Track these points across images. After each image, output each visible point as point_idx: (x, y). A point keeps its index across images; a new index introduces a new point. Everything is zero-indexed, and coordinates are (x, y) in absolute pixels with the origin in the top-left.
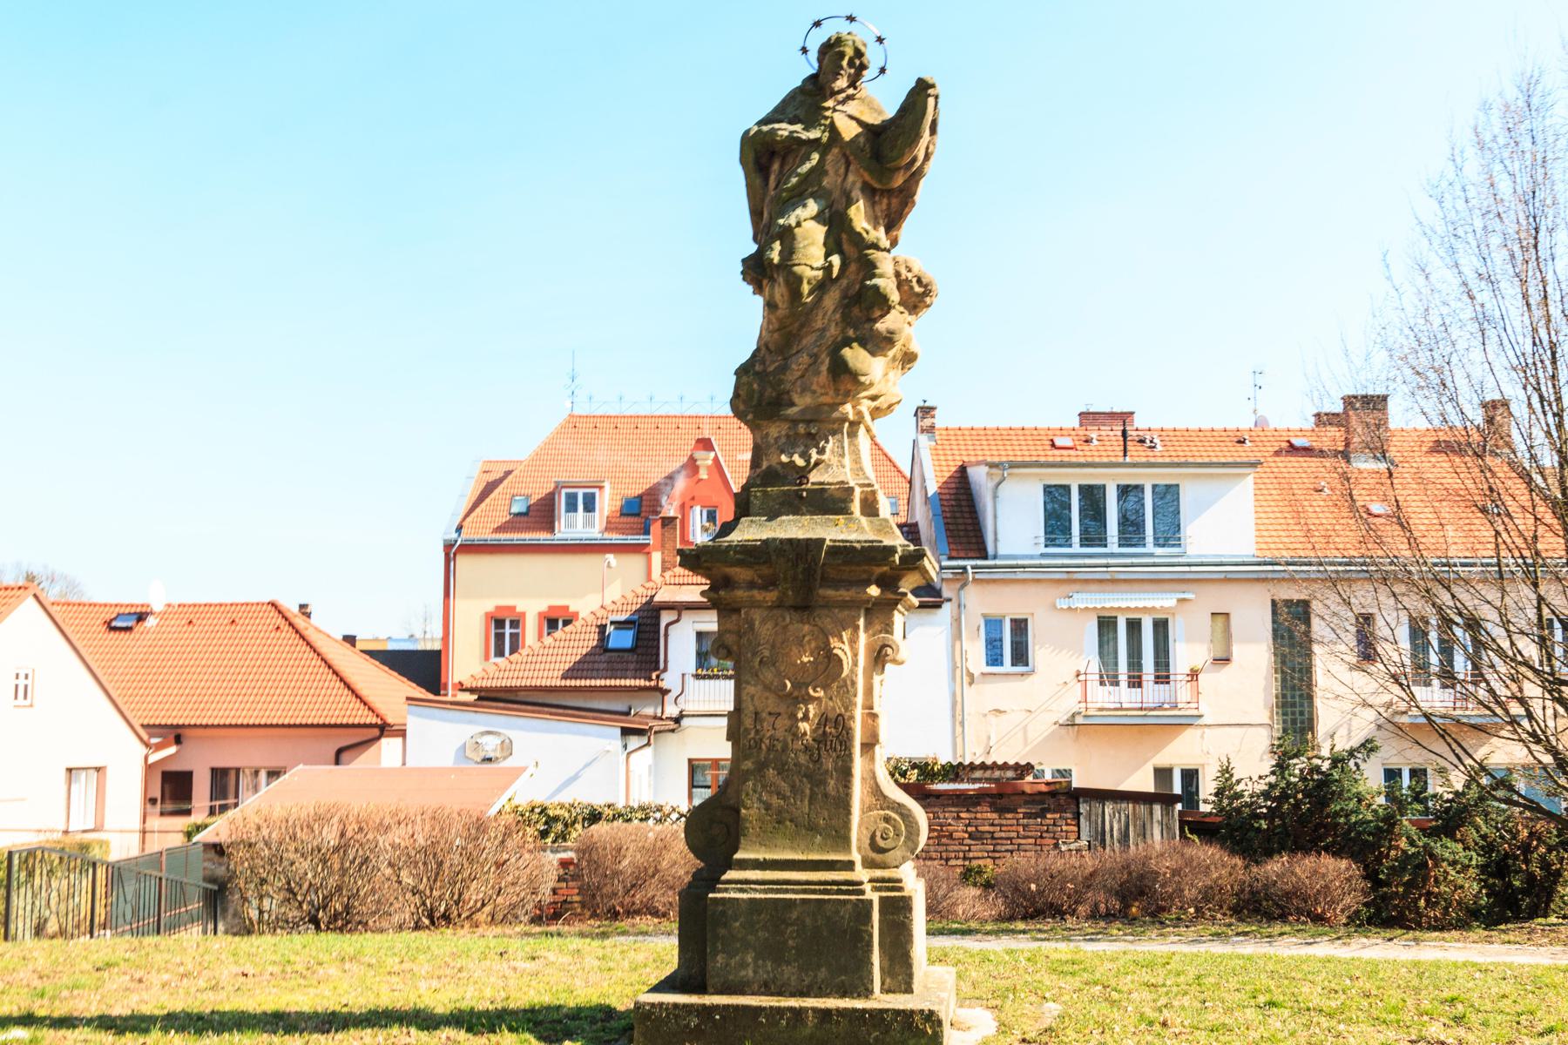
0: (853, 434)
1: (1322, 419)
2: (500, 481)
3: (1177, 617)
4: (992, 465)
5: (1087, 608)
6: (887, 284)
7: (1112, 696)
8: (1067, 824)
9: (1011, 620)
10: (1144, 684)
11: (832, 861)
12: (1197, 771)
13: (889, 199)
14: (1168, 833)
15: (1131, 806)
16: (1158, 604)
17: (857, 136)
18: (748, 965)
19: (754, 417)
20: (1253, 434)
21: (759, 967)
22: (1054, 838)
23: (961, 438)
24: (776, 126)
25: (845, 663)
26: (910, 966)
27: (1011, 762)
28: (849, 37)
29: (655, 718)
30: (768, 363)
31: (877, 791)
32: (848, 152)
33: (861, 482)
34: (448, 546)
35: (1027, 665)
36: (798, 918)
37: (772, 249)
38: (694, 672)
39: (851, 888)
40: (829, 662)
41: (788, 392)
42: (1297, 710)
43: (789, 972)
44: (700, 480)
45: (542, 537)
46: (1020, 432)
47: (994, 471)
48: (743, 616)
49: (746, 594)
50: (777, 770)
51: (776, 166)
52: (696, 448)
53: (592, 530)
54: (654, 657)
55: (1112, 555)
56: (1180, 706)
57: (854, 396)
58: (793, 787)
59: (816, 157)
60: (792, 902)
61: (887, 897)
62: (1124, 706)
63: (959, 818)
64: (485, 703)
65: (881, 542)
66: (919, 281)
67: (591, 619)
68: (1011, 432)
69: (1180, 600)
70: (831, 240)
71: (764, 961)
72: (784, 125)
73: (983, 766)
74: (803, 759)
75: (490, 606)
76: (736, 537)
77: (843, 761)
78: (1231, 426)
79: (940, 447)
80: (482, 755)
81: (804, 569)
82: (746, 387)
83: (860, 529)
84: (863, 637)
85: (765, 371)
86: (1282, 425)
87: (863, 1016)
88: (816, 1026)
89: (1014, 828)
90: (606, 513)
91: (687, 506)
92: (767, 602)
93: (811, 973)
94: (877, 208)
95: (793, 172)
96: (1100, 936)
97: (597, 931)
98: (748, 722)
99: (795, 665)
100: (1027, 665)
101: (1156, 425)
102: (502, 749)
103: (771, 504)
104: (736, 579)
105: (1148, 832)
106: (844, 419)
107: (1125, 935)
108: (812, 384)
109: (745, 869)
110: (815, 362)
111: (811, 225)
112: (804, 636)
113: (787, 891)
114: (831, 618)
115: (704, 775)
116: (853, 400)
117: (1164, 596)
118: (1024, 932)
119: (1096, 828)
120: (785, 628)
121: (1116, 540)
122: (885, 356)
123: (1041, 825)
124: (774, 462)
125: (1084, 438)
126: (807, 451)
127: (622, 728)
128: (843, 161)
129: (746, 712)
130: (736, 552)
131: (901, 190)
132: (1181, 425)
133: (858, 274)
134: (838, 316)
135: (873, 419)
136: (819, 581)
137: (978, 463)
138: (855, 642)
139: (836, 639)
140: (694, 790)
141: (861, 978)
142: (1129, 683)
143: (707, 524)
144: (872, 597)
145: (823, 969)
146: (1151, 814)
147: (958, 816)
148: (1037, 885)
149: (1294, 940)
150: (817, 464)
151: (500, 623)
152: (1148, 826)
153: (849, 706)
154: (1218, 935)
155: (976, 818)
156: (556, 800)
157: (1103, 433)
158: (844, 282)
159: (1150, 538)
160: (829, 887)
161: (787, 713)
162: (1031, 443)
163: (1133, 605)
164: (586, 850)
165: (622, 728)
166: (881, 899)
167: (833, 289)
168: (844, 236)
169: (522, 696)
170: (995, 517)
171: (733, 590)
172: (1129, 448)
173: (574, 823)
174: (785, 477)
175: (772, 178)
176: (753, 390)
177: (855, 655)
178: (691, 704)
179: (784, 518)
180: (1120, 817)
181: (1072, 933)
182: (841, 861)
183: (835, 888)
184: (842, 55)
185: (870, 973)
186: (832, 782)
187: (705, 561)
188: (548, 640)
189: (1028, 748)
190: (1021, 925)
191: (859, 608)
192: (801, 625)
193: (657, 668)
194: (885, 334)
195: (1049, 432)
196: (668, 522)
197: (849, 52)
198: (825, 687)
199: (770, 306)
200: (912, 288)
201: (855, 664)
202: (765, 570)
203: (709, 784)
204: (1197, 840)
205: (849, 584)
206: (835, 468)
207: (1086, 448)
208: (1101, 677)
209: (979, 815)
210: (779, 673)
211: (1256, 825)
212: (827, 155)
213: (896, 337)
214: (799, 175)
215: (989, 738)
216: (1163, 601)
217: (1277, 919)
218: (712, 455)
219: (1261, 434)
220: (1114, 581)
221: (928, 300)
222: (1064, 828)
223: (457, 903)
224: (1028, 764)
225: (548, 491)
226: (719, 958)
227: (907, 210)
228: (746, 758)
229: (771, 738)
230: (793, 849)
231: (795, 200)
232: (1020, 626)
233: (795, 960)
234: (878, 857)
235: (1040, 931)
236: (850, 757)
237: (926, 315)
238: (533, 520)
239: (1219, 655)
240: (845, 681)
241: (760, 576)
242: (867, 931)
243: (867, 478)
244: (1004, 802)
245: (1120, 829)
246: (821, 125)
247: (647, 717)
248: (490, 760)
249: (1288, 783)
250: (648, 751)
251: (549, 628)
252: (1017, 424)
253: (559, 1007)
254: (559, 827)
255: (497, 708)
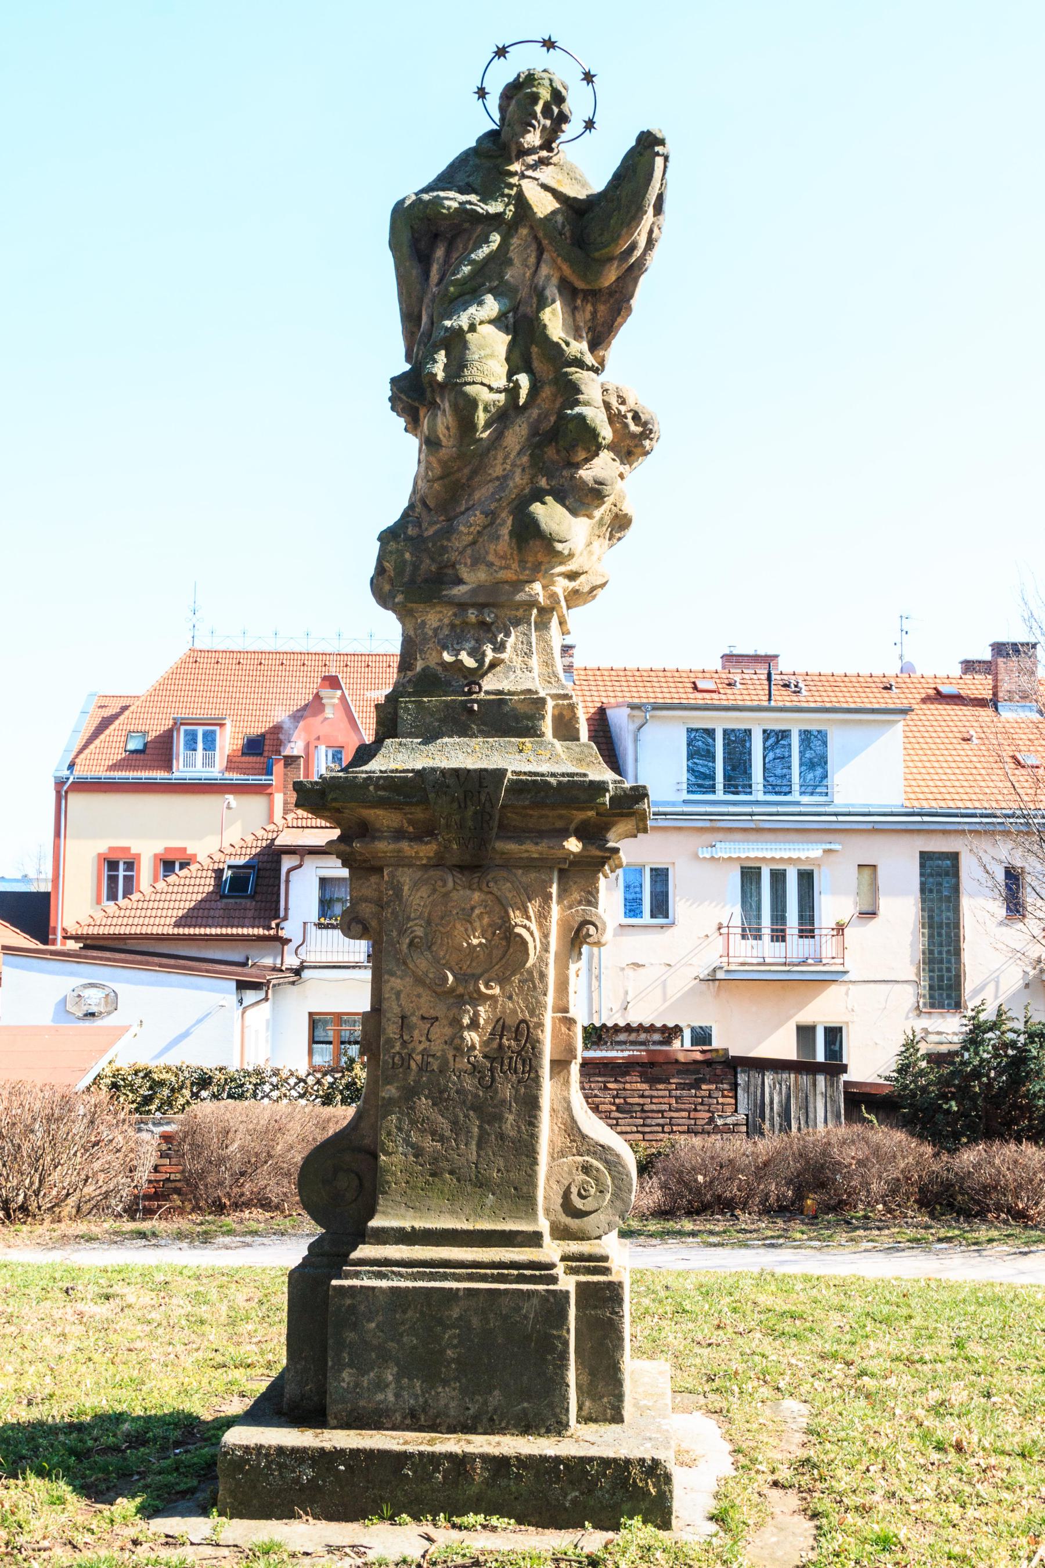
0: (543, 626)
1: (969, 666)
2: (115, 717)
3: (822, 868)
4: (633, 707)
5: (730, 858)
6: (596, 416)
7: (755, 951)
8: (723, 1096)
9: (652, 870)
10: (788, 938)
11: (511, 1231)
12: (840, 1029)
13: (594, 305)
14: (832, 1106)
15: (792, 1076)
16: (803, 855)
17: (554, 213)
18: (387, 1386)
19: (405, 598)
20: (899, 680)
21: (402, 1388)
22: (709, 1111)
23: (599, 678)
24: (442, 194)
25: (531, 946)
26: (619, 1383)
27: (659, 1025)
28: (545, 75)
29: (274, 969)
30: (425, 525)
31: (572, 1130)
32: (541, 235)
33: (554, 691)
34: (60, 783)
35: (667, 917)
36: (460, 1318)
37: (435, 361)
38: (317, 921)
39: (537, 1273)
40: (508, 946)
41: (453, 566)
42: (944, 966)
43: (447, 1397)
44: (326, 719)
45: (159, 775)
46: (661, 674)
47: (636, 713)
48: (386, 878)
49: (392, 847)
50: (432, 1099)
51: (440, 253)
52: (322, 686)
53: (212, 769)
54: (275, 896)
55: (757, 803)
56: (824, 961)
57: (546, 572)
58: (455, 1123)
59: (496, 239)
60: (451, 1295)
61: (588, 1283)
62: (767, 960)
63: (606, 1088)
64: (95, 953)
65: (585, 775)
66: (636, 417)
67: (207, 863)
68: (652, 674)
69: (826, 851)
70: (517, 354)
71: (410, 1379)
72: (451, 194)
73: (628, 1028)
74: (469, 1083)
75: (102, 846)
76: (377, 765)
77: (526, 1087)
78: (877, 672)
79: (577, 688)
80: (85, 1009)
81: (476, 813)
82: (394, 556)
83: (553, 757)
84: (556, 910)
85: (420, 536)
86: (929, 673)
87: (557, 1467)
88: (486, 1483)
89: (666, 1100)
90: (227, 753)
91: (312, 747)
92: (421, 858)
93: (478, 1397)
94: (579, 316)
95: (464, 259)
96: (781, 1241)
97: (198, 1229)
98: (391, 1030)
99: (460, 948)
100: (667, 917)
101: (801, 669)
102: (106, 1003)
103: (427, 720)
104: (378, 826)
105: (811, 1105)
106: (532, 603)
107: (810, 1239)
108: (487, 553)
109: (385, 1243)
110: (491, 524)
111: (488, 331)
112: (473, 909)
113: (445, 1277)
114: (512, 883)
115: (325, 1030)
116: (544, 577)
117: (810, 846)
118: (693, 1234)
119: (755, 1100)
120: (446, 895)
121: (761, 787)
122: (590, 516)
123: (696, 1096)
124: (432, 662)
125: (726, 681)
126: (480, 648)
127: (238, 981)
128: (534, 247)
129: (389, 1015)
130: (378, 787)
131: (611, 292)
132: (826, 670)
133: (554, 401)
134: (525, 459)
135: (568, 608)
136: (495, 830)
137: (618, 705)
138: (545, 918)
139: (518, 913)
140: (315, 1046)
141: (551, 1406)
142: (772, 937)
143: (333, 765)
144: (573, 853)
145: (496, 1393)
146: (815, 1085)
147: (605, 1086)
148: (705, 1176)
149: (1005, 1248)
150: (493, 665)
151: (113, 865)
152: (811, 1099)
153: (535, 1008)
154: (917, 1240)
155: (624, 1089)
156: (162, 1062)
157: (746, 676)
158: (535, 413)
159: (796, 787)
160: (506, 1272)
161: (446, 1017)
162: (672, 685)
163: (778, 855)
164: (191, 1132)
165: (238, 981)
166: (579, 1285)
167: (519, 421)
168: (534, 349)
169: (132, 945)
170: (636, 760)
171: (374, 838)
172: (773, 692)
173: (181, 1088)
174: (448, 683)
175: (435, 269)
176: (404, 562)
177: (546, 936)
178: (312, 954)
179: (446, 740)
180: (781, 1089)
181: (748, 1235)
182: (522, 1232)
183: (515, 1272)
184: (535, 98)
185: (565, 1398)
186: (511, 1117)
187: (334, 800)
188: (161, 885)
189: (667, 1004)
190: (688, 1225)
191: (551, 868)
192: (468, 892)
193: (277, 916)
194: (591, 483)
195: (692, 675)
196: (291, 761)
197: (545, 94)
198: (502, 981)
199: (431, 443)
200: (626, 426)
201: (546, 949)
202: (419, 814)
203: (331, 1039)
204: (875, 1121)
205: (539, 834)
206: (518, 672)
207: (729, 691)
208: (744, 930)
209: (628, 1086)
210: (437, 960)
211: (945, 1106)
212: (512, 237)
213: (607, 490)
214: (472, 262)
215: (626, 993)
216: (809, 852)
217: (975, 1217)
218: (339, 693)
219: (908, 680)
220: (758, 830)
221: (647, 443)
222: (721, 1100)
223: (37, 1193)
224: (677, 1026)
225: (166, 728)
226: (345, 1375)
227: (619, 320)
228: (388, 1081)
229: (425, 1053)
230: (453, 1213)
231: (467, 297)
232: (660, 876)
233: (457, 1379)
234: (573, 1223)
235: (711, 1233)
236: (537, 1081)
237: (644, 466)
238: (150, 757)
239: (865, 909)
240: (530, 972)
241: (410, 822)
242: (560, 1337)
243: (563, 687)
244: (656, 1070)
245: (780, 1102)
246: (503, 195)
247: (265, 968)
248: (93, 1014)
249: (982, 1060)
250: (266, 1006)
251: (165, 871)
252: (658, 666)
253: (119, 1418)
254: (166, 1092)
255: (101, 959)
